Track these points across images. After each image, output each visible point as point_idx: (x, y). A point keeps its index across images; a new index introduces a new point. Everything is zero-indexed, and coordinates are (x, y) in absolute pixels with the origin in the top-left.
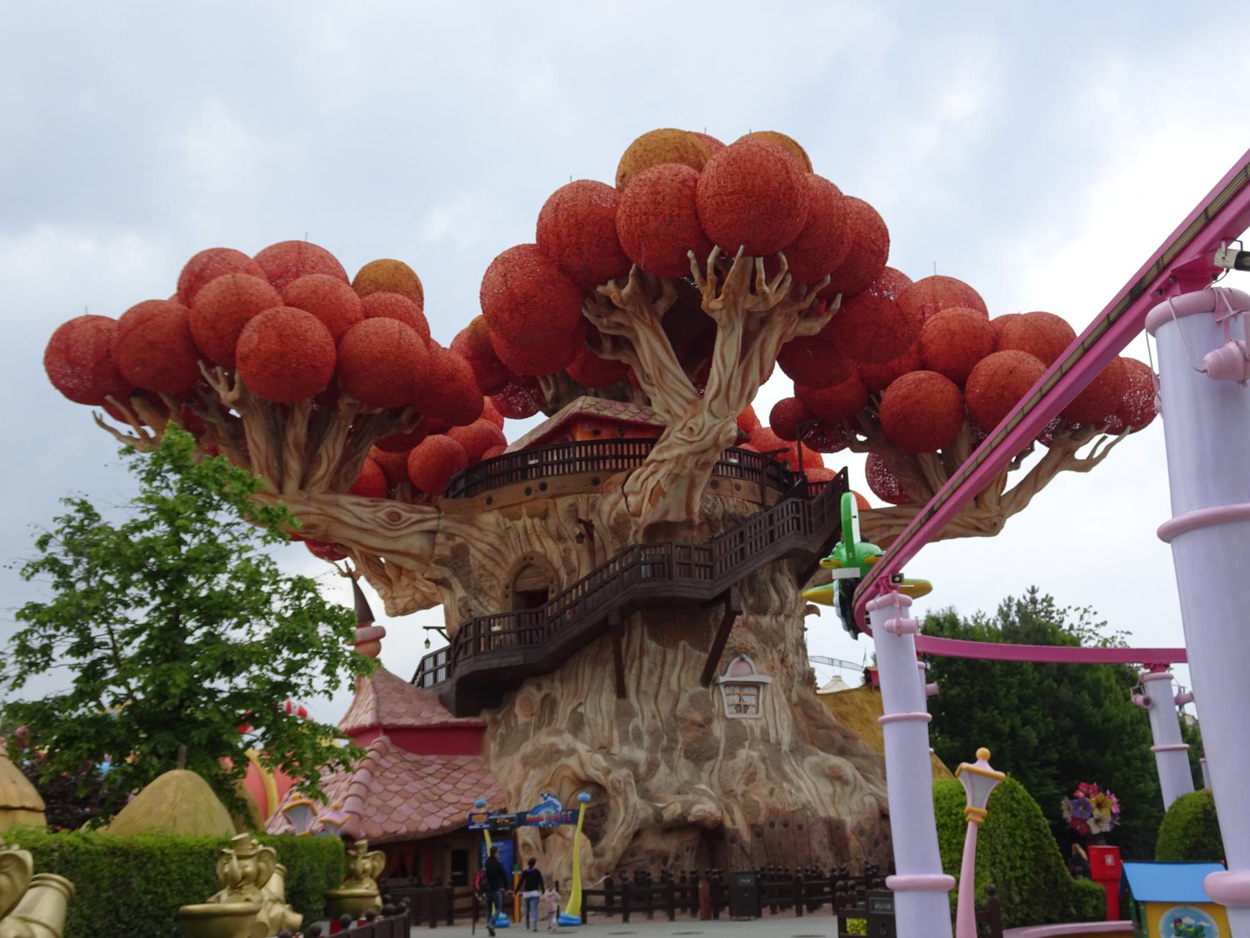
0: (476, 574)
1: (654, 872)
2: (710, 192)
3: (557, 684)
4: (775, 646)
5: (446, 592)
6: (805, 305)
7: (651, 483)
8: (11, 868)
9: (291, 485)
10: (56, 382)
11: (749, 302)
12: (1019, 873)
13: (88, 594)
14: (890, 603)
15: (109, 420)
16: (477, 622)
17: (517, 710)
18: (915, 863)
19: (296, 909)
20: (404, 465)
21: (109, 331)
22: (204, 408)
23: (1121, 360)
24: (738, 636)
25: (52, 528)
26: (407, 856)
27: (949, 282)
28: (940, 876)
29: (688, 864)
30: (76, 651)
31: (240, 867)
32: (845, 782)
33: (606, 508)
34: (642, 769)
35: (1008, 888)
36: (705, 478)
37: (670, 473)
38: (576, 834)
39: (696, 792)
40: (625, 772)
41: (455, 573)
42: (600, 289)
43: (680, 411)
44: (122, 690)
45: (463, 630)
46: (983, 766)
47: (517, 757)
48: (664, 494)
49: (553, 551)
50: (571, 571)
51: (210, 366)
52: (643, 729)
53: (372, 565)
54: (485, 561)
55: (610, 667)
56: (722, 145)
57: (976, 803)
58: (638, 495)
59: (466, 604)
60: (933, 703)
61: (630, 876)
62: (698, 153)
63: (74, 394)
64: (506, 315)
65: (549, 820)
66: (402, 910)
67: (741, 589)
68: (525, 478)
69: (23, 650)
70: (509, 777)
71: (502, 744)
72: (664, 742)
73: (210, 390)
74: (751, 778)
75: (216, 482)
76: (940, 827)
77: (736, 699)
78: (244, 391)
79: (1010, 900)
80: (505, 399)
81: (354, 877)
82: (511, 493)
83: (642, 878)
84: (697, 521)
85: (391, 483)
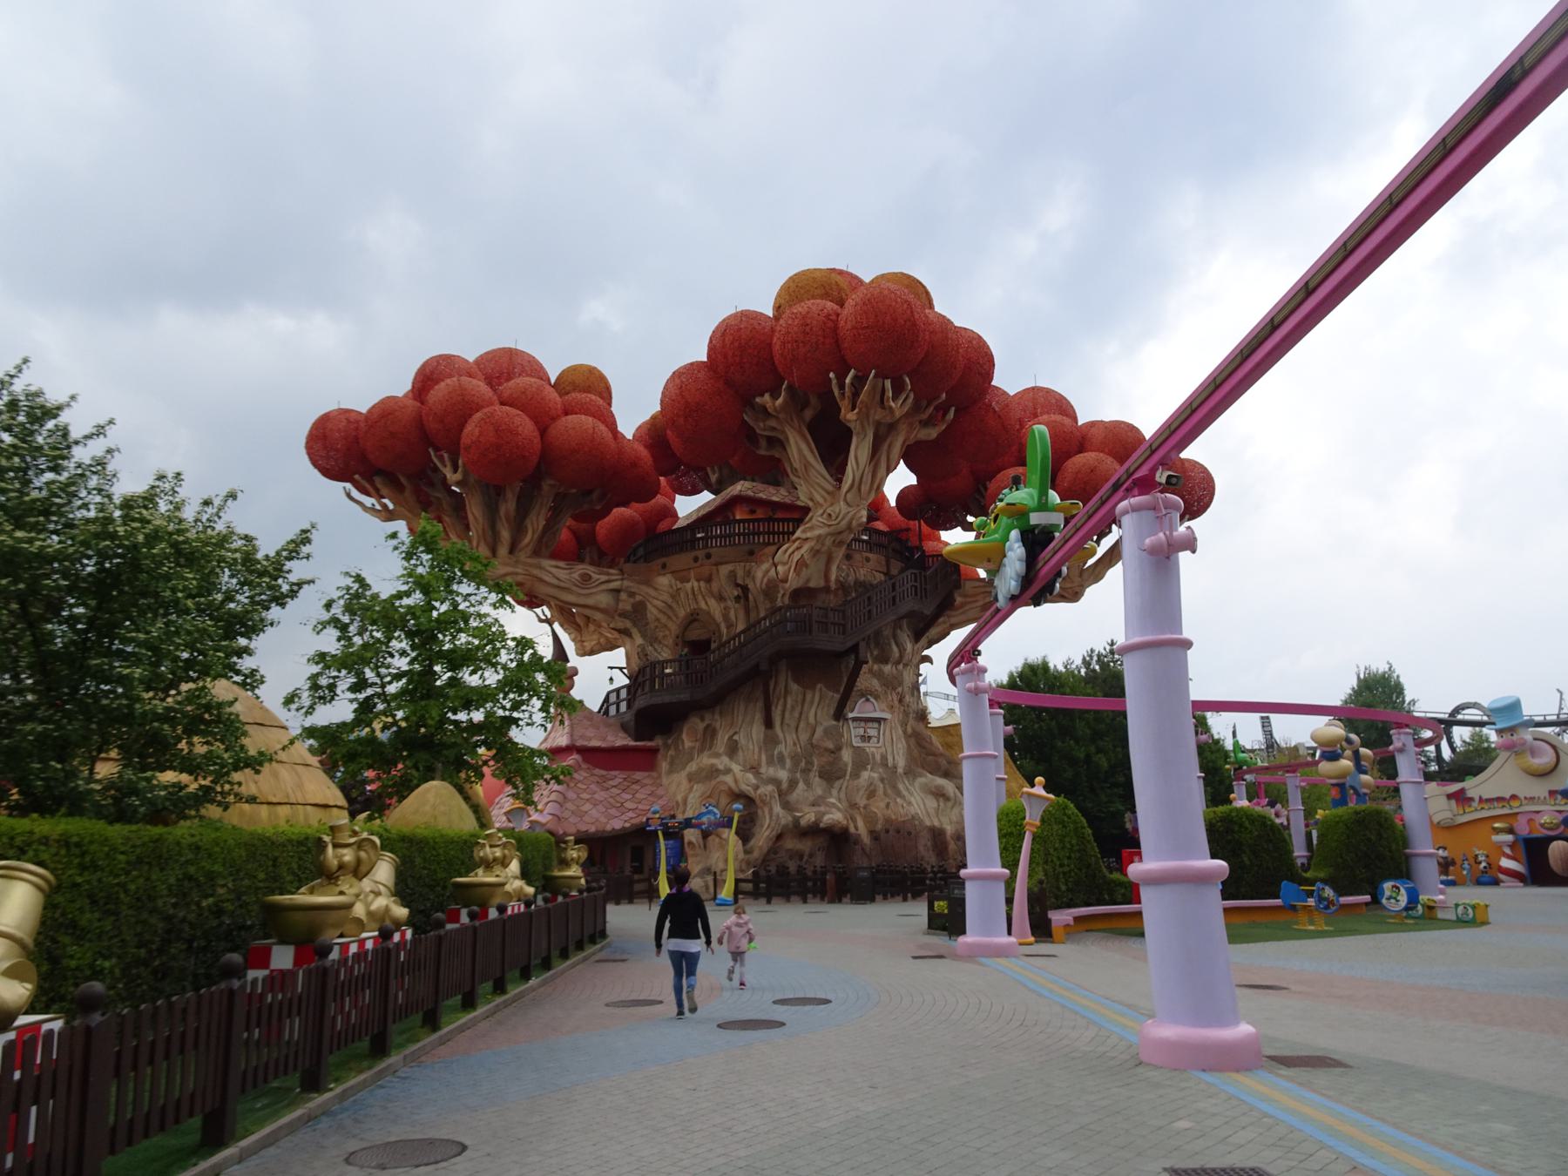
0: (652, 626)
1: (792, 867)
2: (849, 326)
3: (717, 717)
4: (894, 689)
5: (627, 640)
6: (924, 416)
7: (797, 556)
8: (368, 847)
9: (503, 551)
10: (315, 464)
11: (878, 415)
12: (1066, 869)
13: (365, 646)
14: (971, 671)
15: (355, 493)
16: (653, 665)
17: (684, 736)
18: (982, 861)
19: (529, 884)
20: (593, 533)
21: (357, 422)
22: (431, 484)
23: (1183, 461)
24: (865, 681)
25: (335, 595)
26: (601, 847)
27: (1048, 392)
28: (1000, 870)
29: (819, 860)
30: (355, 688)
31: (336, 856)
32: (946, 798)
33: (759, 574)
34: (785, 786)
35: (1057, 880)
36: (840, 553)
37: (812, 549)
38: (731, 836)
39: (827, 805)
40: (770, 788)
41: (635, 625)
42: (758, 400)
43: (821, 500)
44: (390, 720)
45: (641, 671)
46: (1039, 790)
47: (684, 774)
48: (807, 566)
49: (715, 608)
50: (730, 626)
51: (437, 450)
52: (786, 754)
53: (565, 614)
54: (660, 616)
55: (760, 704)
56: (861, 281)
57: (1033, 817)
58: (787, 564)
59: (643, 649)
60: (1009, 744)
61: (773, 869)
62: (840, 290)
63: (330, 473)
64: (681, 421)
65: (710, 824)
66: (601, 888)
67: (868, 644)
68: (693, 548)
69: (315, 687)
70: (678, 789)
71: (672, 764)
72: (803, 764)
73: (436, 469)
74: (871, 794)
75: (459, 561)
76: (1002, 836)
77: (861, 731)
78: (465, 474)
79: (1058, 888)
80: (677, 478)
81: (565, 863)
82: (681, 560)
83: (783, 870)
84: (833, 586)
85: (582, 549)
